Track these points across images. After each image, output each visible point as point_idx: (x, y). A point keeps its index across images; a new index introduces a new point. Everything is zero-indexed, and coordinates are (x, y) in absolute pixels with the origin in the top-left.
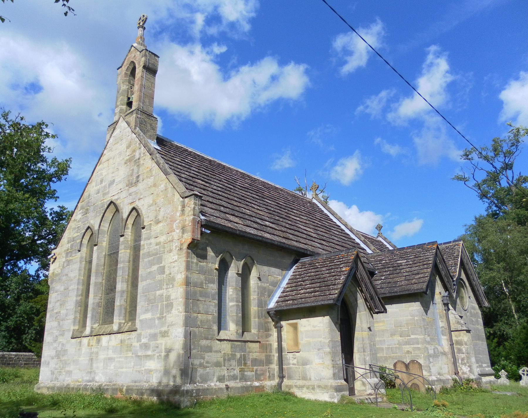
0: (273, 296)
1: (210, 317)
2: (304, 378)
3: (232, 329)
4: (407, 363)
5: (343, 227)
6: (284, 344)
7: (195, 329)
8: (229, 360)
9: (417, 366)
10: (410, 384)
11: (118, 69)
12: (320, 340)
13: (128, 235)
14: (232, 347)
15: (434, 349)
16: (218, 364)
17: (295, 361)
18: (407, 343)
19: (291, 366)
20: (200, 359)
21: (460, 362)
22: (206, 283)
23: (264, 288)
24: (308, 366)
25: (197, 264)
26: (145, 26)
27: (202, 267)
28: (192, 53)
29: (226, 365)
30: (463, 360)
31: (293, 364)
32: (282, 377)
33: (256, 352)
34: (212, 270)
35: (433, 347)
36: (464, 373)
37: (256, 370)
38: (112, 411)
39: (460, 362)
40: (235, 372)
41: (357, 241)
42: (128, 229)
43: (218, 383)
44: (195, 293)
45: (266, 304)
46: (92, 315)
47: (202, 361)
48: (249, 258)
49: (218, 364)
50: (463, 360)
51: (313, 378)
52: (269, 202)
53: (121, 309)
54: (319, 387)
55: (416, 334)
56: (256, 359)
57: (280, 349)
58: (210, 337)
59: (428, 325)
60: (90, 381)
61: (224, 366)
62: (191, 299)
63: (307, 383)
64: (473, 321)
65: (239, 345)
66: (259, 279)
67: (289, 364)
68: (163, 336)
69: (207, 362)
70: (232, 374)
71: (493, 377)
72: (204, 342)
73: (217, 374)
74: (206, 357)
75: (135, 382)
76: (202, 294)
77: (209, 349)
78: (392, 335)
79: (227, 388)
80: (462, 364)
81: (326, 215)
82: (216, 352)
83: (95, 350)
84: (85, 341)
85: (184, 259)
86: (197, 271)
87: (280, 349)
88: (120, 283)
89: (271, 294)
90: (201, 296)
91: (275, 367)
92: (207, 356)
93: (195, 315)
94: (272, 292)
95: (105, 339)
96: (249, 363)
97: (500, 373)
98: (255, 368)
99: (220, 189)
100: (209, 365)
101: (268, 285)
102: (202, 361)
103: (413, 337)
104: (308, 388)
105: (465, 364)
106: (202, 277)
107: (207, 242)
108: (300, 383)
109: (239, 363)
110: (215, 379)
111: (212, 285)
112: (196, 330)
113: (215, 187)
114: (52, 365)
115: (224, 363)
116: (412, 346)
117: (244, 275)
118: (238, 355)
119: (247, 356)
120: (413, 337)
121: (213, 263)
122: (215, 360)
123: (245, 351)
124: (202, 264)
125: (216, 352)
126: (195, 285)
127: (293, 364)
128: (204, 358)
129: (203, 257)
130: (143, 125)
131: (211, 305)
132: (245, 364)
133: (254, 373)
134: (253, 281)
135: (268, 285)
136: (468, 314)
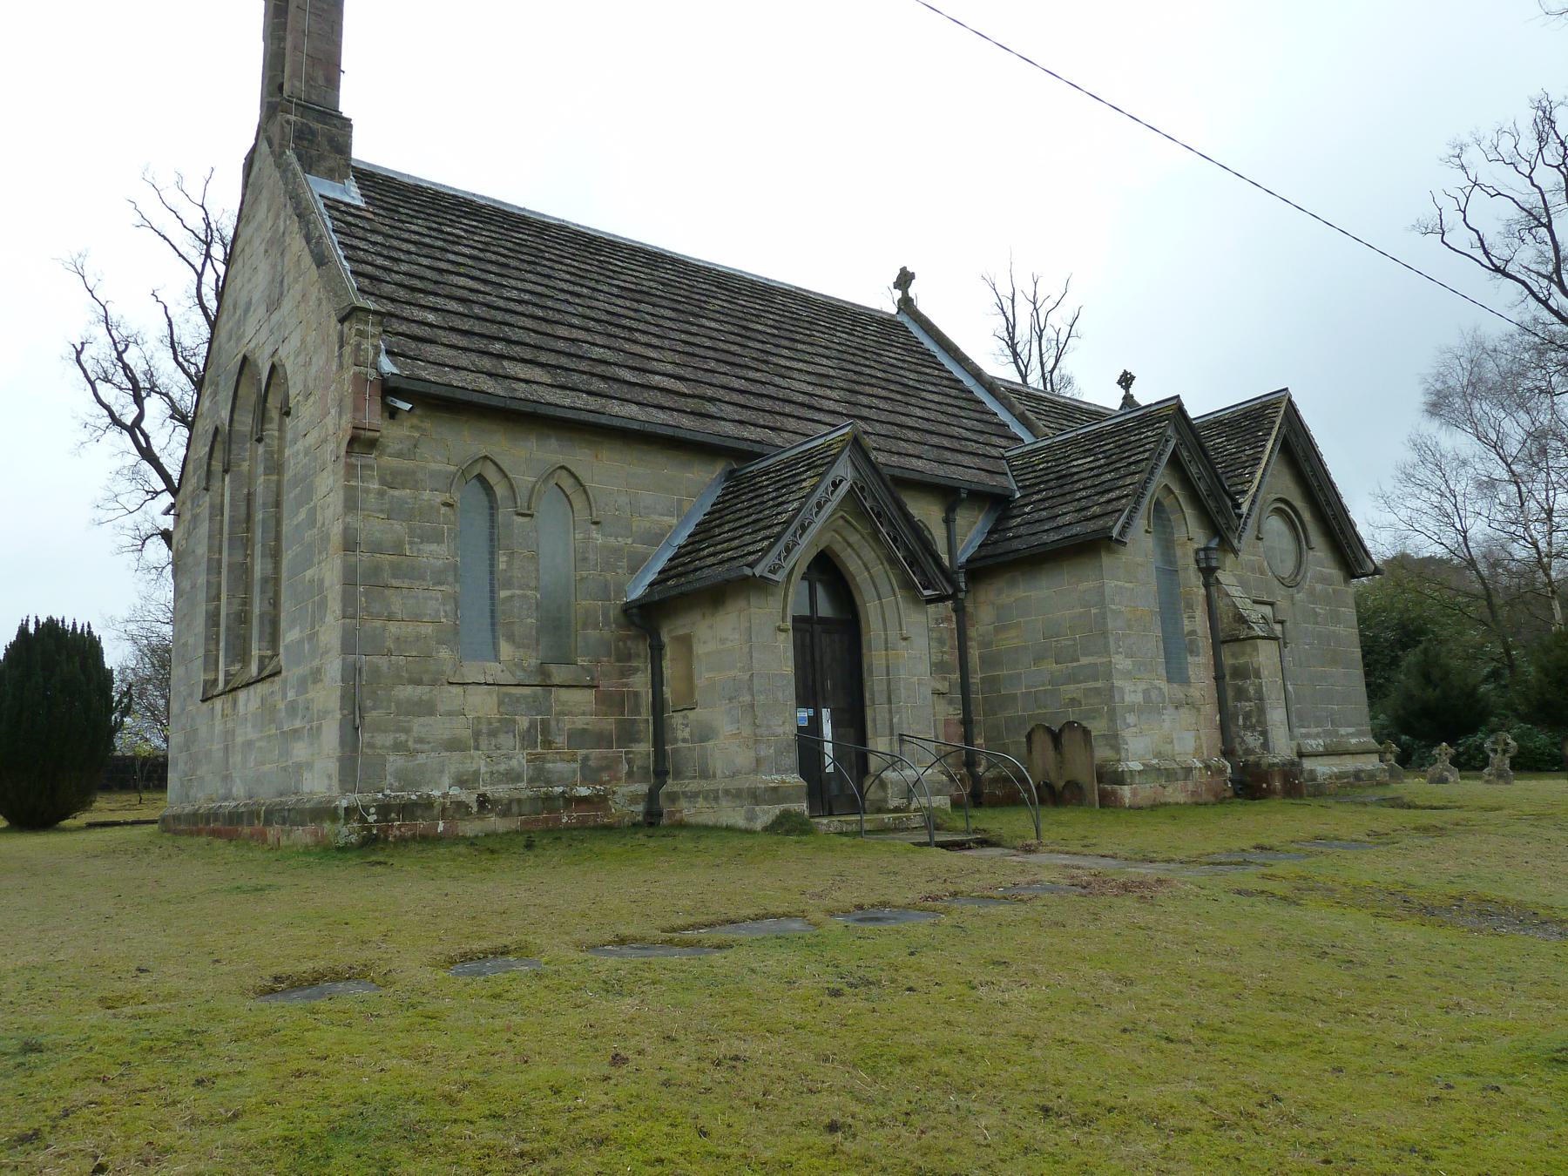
0: (647, 569)
2: (705, 774)
4: (1056, 729)
5: (969, 382)
6: (668, 692)
7: (375, 659)
8: (493, 734)
9: (1079, 735)
10: (1062, 783)
12: (732, 673)
13: (272, 437)
14: (501, 703)
15: (1146, 692)
16: (454, 745)
17: (686, 734)
18: (1072, 678)
19: (681, 744)
20: (396, 731)
21: (1241, 722)
22: (411, 543)
24: (710, 744)
25: (381, 494)
29: (483, 745)
30: (1247, 716)
31: (684, 740)
32: (661, 774)
33: (584, 714)
34: (432, 507)
35: (1142, 686)
36: (1248, 752)
37: (586, 758)
39: (1241, 722)
40: (514, 763)
41: (1004, 416)
42: (271, 420)
43: (455, 791)
46: (227, 643)
47: (403, 737)
48: (564, 473)
49: (454, 745)
50: (1247, 716)
51: (719, 773)
52: (713, 325)
53: (262, 623)
54: (727, 792)
55: (1092, 655)
56: (584, 731)
57: (658, 706)
58: (426, 678)
59: (1130, 627)
60: (226, 799)
61: (477, 748)
63: (706, 785)
64: (1316, 614)
65: (525, 697)
67: (676, 740)
68: (315, 681)
69: (421, 741)
70: (503, 767)
71: (1375, 758)
72: (407, 692)
74: (415, 728)
75: (281, 795)
77: (428, 709)
78: (1038, 659)
80: (1246, 727)
81: (928, 353)
82: (450, 714)
83: (230, 725)
84: (218, 703)
85: (342, 482)
86: (382, 511)
87: (658, 706)
88: (1200, 633)
90: (395, 576)
91: (644, 748)
92: (419, 725)
93: (378, 623)
94: (645, 559)
95: (242, 695)
96: (560, 740)
97: (1436, 751)
98: (582, 752)
99: (527, 297)
100: (426, 747)
101: (629, 541)
102: (403, 737)
103: (1084, 661)
104: (706, 798)
105: (1253, 728)
106: (399, 527)
107: (417, 435)
108: (693, 786)
109: (528, 739)
110: (446, 781)
111: (434, 547)
112: (382, 662)
113: (514, 294)
114: (181, 766)
115: (476, 740)
116: (1082, 685)
118: (523, 722)
119: (553, 723)
120: (1084, 661)
122: (446, 735)
123: (549, 711)
124: (397, 493)
125: (450, 714)
127: (684, 740)
128: (407, 731)
130: (305, 143)
131: (431, 598)
132: (548, 744)
133: (577, 766)
135: (629, 541)
136: (1299, 596)
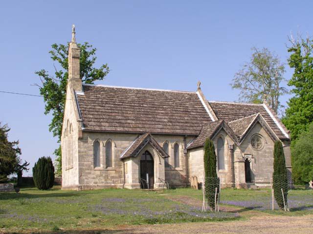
1: (90, 163)
3: (102, 166)
11: (289, 51)
16: (94, 178)
23: (119, 151)
26: (75, 31)
27: (85, 146)
28: (191, 168)
38: (33, 233)
44: (82, 155)
45: (119, 156)
49: (94, 178)
62: (81, 157)
66: (116, 147)
72: (87, 171)
73: (94, 181)
76: (87, 155)
77: (90, 173)
79: (98, 186)
89: (122, 152)
92: (89, 176)
106: (86, 149)
117: (108, 146)
118: (104, 175)
121: (91, 142)
126: (82, 152)
129: (86, 142)
132: (107, 178)
134: (113, 148)
